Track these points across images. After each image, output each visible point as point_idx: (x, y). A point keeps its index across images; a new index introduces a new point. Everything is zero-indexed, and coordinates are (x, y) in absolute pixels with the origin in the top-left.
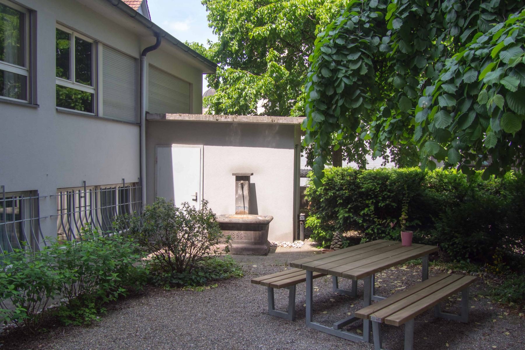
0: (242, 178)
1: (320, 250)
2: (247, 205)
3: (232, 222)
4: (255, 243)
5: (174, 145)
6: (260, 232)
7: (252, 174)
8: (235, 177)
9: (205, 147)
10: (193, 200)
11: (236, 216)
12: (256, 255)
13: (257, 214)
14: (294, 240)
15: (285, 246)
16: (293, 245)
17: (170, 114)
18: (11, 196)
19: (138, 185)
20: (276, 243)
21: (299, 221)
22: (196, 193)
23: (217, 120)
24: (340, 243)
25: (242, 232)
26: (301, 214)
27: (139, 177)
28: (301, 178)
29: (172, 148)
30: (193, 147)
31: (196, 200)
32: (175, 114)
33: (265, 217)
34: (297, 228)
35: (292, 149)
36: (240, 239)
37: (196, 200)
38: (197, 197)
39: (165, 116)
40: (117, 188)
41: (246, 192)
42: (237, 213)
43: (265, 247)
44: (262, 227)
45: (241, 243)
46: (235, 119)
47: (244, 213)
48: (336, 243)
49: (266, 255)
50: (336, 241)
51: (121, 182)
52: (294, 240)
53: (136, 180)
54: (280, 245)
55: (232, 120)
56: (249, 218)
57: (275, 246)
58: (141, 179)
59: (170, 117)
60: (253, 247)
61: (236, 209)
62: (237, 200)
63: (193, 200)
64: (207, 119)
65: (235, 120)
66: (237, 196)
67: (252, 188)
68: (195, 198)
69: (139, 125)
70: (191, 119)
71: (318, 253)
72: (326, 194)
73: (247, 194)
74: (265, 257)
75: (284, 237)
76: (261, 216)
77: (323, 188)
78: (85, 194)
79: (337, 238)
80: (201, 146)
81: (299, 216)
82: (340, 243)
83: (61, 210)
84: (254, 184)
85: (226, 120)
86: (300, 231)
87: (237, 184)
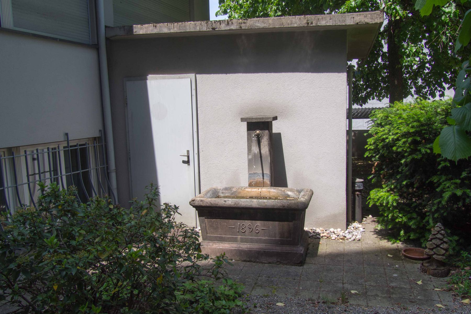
0: (259, 126)
1: (395, 245)
2: (267, 171)
3: (239, 206)
4: (282, 243)
5: (150, 77)
6: (291, 224)
7: (275, 118)
8: (245, 124)
9: (197, 75)
10: (184, 162)
11: (249, 190)
12: (284, 264)
13: (287, 187)
14: (348, 223)
15: (334, 236)
16: (348, 236)
17: (139, 26)
18: (84, 143)
19: (100, 140)
20: (318, 230)
21: (354, 191)
22: (188, 151)
23: (214, 29)
24: (445, 246)
25: (258, 223)
26: (358, 180)
27: (101, 128)
28: (353, 120)
29: (148, 82)
30: (179, 78)
31: (188, 162)
32: (147, 25)
33: (299, 192)
34: (350, 202)
35: (343, 72)
36: (252, 237)
37: (188, 162)
38: (188, 157)
39: (131, 29)
40: (61, 148)
41: (265, 150)
42: (250, 185)
43: (301, 250)
44: (292, 214)
45: (258, 241)
46: (243, 25)
47: (262, 185)
48: (438, 246)
49: (301, 263)
50: (438, 242)
51: (62, 138)
52: (348, 223)
53: (97, 135)
54: (325, 234)
55: (238, 27)
56: (269, 195)
57: (317, 237)
58: (104, 131)
59: (141, 30)
60: (278, 249)
61: (250, 177)
62: (250, 162)
63: (184, 162)
64: (198, 29)
65: (244, 27)
66: (250, 157)
67: (276, 143)
68: (186, 159)
69: (96, 47)
70: (172, 31)
71: (395, 252)
72: (413, 151)
73: (268, 153)
74: (299, 269)
75: (331, 221)
76: (291, 190)
77: (410, 140)
78: (38, 155)
79: (439, 236)
80: (192, 76)
81: (354, 183)
82: (445, 246)
83: (39, 173)
84: (279, 134)
85: (228, 28)
86: (358, 206)
87: (248, 135)
